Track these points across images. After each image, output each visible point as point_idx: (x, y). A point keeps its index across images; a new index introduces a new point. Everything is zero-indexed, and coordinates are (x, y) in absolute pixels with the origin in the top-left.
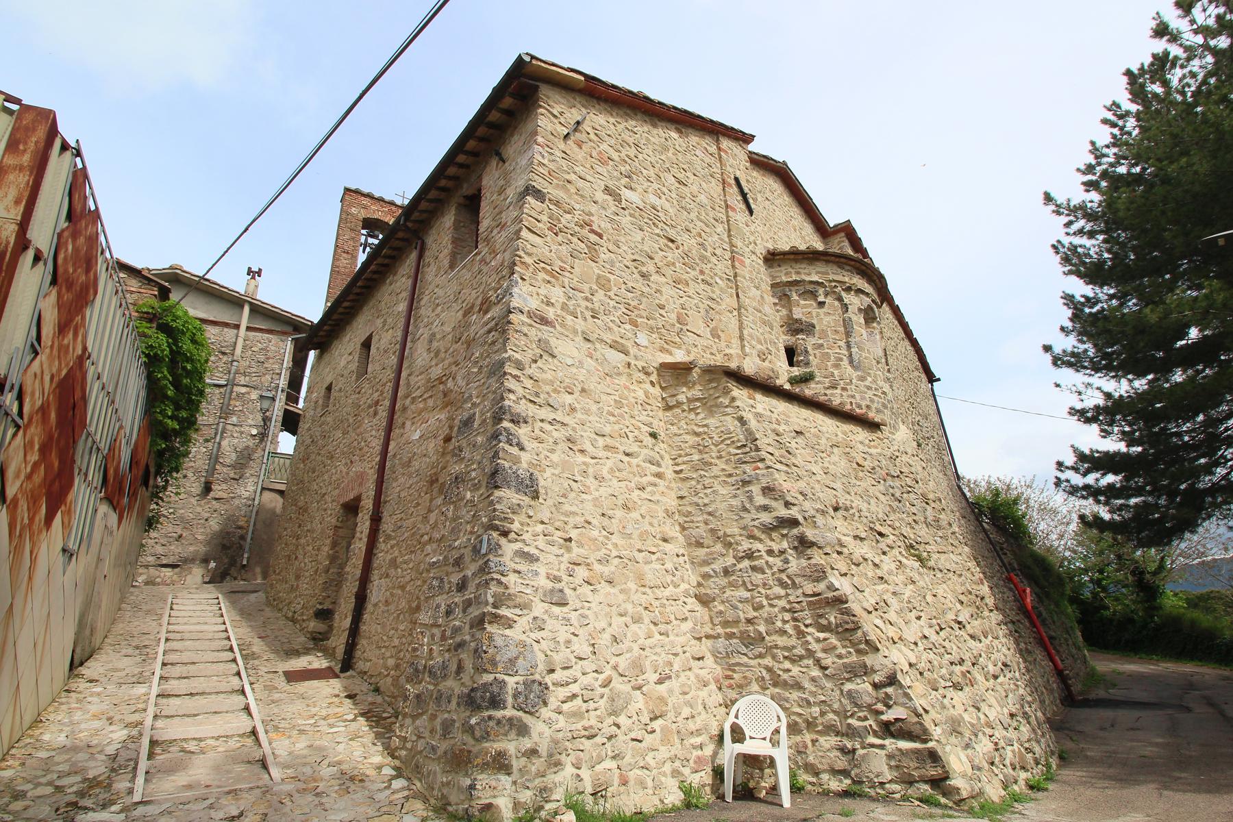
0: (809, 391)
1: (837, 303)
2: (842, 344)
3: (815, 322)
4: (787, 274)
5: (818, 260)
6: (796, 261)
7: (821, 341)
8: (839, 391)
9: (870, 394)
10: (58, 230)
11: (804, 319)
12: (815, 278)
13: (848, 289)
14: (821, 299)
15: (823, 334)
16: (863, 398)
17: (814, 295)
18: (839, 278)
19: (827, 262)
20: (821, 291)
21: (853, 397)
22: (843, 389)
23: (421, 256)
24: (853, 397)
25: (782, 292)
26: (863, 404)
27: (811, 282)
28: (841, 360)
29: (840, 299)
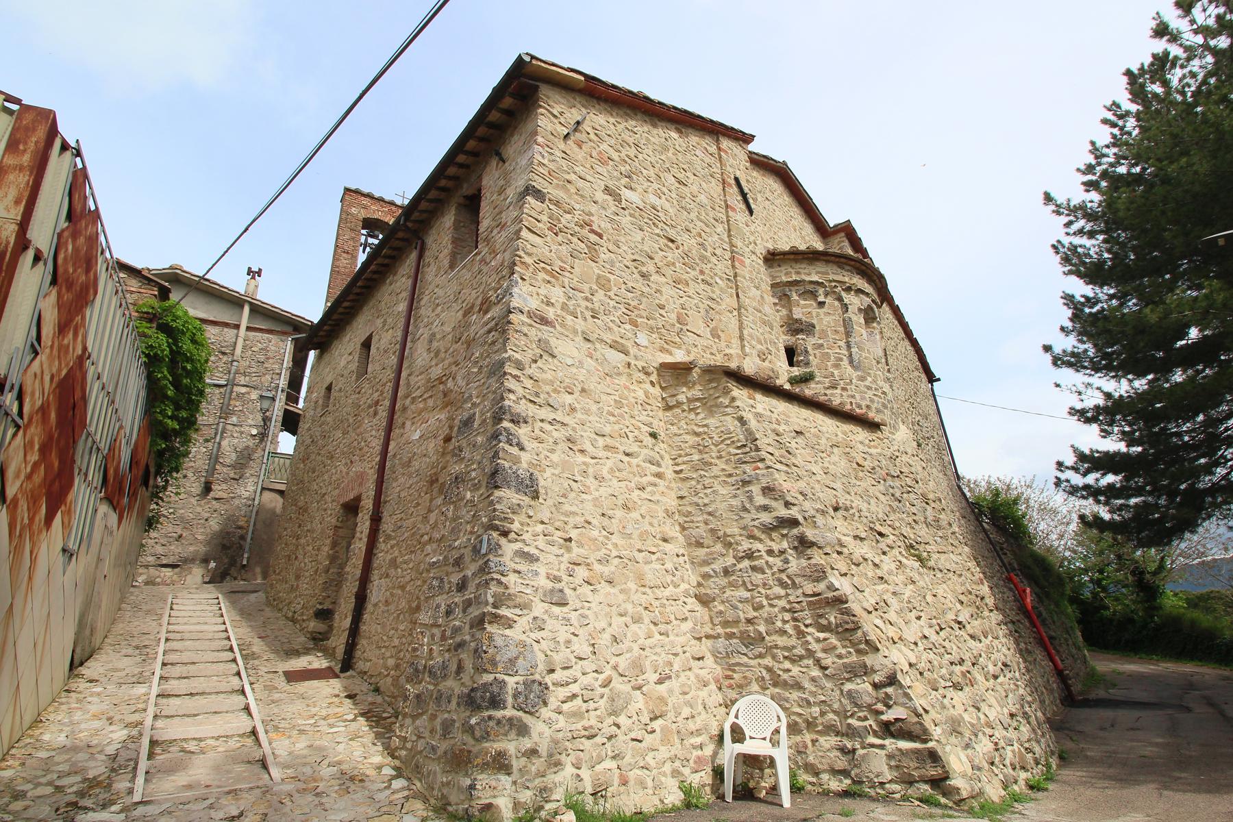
0: (809, 391)
1: (837, 303)
2: (842, 344)
3: (815, 322)
4: (787, 274)
5: (818, 260)
6: (796, 261)
7: (821, 341)
8: (839, 391)
9: (870, 394)
10: (58, 230)
11: (804, 319)
12: (815, 278)
13: (848, 289)
14: (821, 299)
15: (823, 334)
16: (863, 398)
17: (814, 295)
18: (839, 278)
19: (827, 262)
20: (821, 291)
21: (853, 397)
22: (843, 389)
23: (421, 256)
24: (853, 397)
25: (782, 292)
26: (863, 404)
27: (811, 282)
28: (841, 360)
29: (840, 299)
